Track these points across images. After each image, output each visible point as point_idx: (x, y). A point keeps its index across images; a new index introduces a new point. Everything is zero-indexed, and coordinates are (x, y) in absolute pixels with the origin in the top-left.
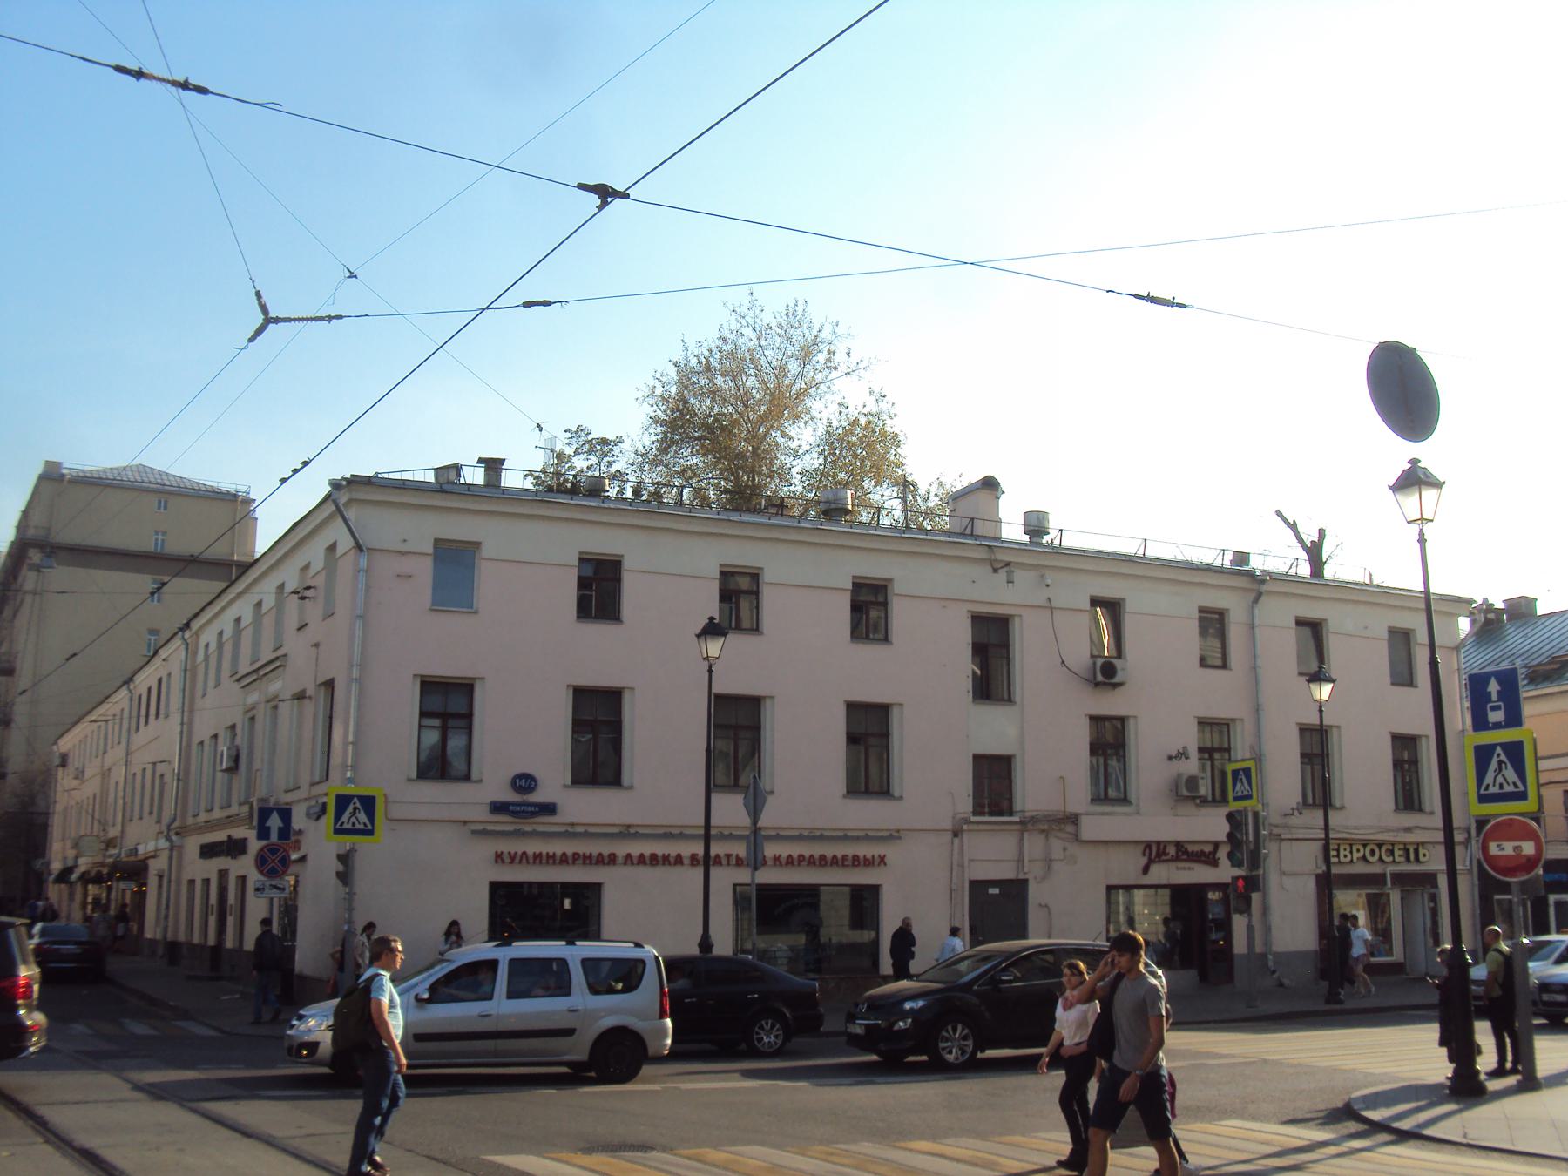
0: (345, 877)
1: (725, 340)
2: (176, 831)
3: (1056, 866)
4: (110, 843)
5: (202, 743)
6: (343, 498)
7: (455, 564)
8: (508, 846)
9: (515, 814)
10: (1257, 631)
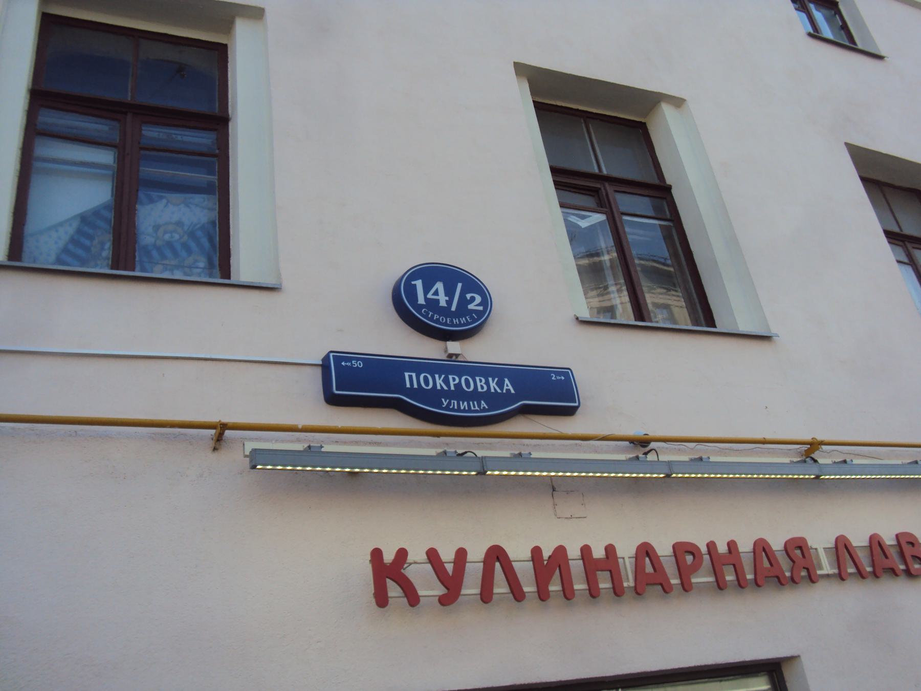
8: (421, 532)
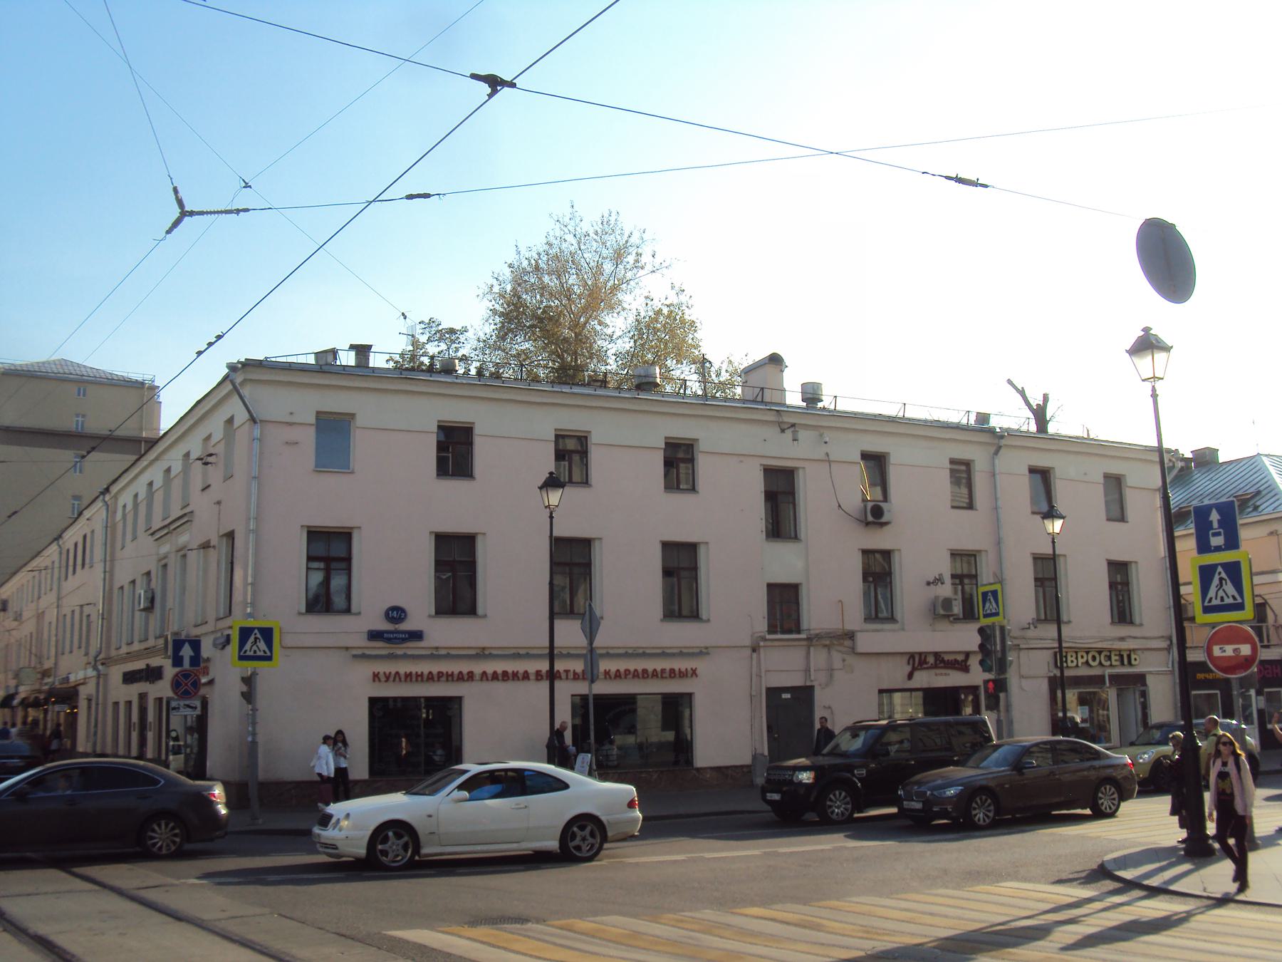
0: (248, 696)
1: (550, 245)
2: (102, 662)
3: (837, 674)
4: (45, 674)
5: (122, 588)
6: (239, 378)
7: (333, 432)
9: (389, 640)
10: (998, 477)
